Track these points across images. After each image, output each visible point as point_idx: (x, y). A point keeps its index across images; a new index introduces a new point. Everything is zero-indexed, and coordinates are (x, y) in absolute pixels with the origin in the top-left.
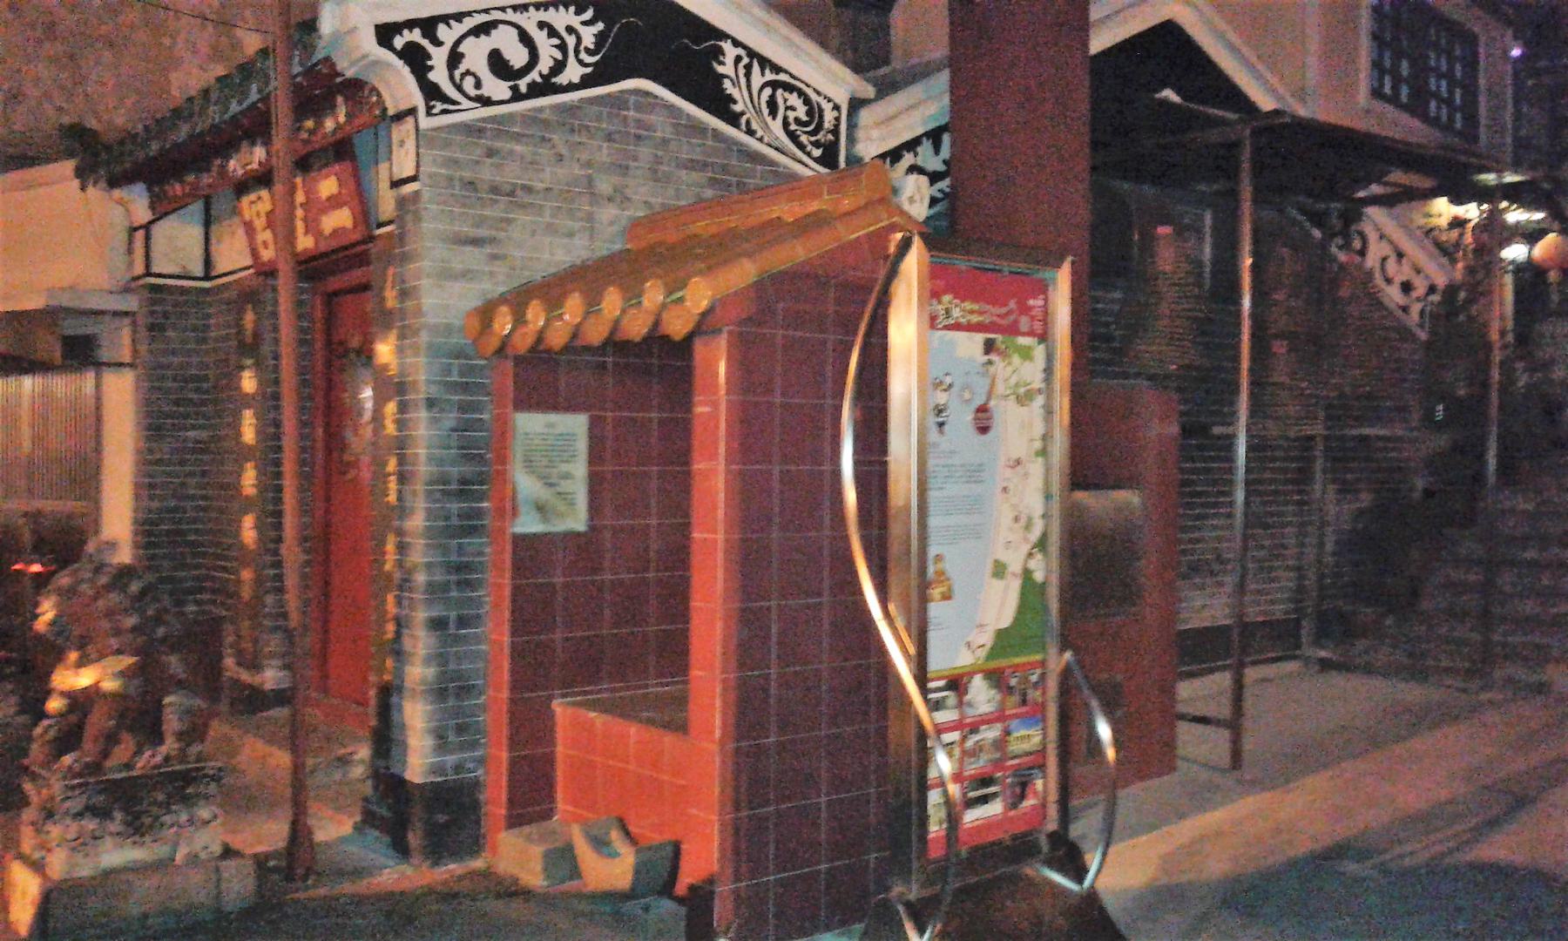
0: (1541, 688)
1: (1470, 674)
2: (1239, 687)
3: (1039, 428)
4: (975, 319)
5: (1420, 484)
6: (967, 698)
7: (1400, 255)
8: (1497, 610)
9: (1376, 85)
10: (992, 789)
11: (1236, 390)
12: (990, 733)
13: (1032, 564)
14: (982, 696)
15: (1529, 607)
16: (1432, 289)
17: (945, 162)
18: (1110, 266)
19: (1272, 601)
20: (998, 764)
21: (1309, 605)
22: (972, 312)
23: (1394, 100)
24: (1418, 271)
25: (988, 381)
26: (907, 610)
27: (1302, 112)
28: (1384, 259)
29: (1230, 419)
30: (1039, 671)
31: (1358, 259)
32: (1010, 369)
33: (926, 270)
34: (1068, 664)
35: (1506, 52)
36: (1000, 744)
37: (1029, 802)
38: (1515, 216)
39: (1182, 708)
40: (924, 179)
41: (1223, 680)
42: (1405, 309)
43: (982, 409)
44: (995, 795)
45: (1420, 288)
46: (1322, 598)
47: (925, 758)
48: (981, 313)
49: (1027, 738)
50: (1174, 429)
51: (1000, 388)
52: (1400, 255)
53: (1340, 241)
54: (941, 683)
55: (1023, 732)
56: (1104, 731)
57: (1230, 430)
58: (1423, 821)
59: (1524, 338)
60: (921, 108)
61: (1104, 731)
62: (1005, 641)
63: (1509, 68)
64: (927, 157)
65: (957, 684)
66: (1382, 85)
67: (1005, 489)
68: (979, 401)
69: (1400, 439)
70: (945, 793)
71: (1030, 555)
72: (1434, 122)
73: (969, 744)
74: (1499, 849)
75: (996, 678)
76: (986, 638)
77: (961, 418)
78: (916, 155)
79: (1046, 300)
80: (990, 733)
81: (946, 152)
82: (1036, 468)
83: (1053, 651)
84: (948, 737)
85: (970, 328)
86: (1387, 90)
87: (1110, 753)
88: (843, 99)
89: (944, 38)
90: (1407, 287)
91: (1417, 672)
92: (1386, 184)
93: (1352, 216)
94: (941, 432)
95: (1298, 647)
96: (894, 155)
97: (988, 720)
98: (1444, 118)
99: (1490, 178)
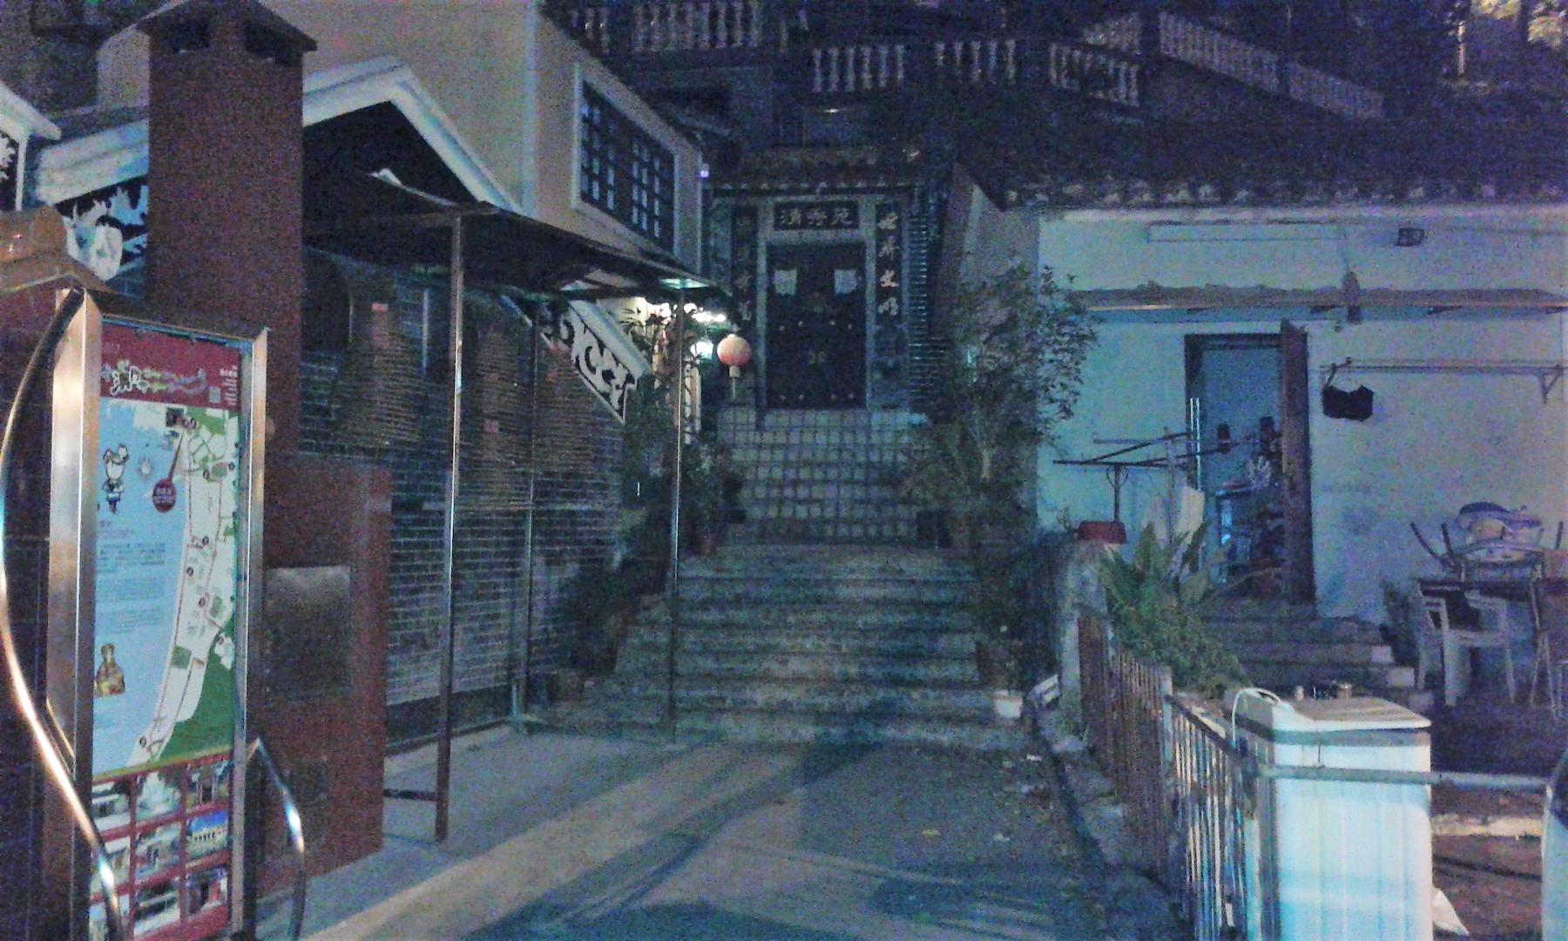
0: (713, 737)
1: (662, 727)
2: (445, 754)
3: (230, 506)
4: (156, 387)
5: (618, 557)
6: (140, 800)
7: (602, 346)
8: (682, 667)
9: (586, 188)
10: (169, 895)
11: (449, 466)
12: (166, 836)
13: (219, 650)
14: (157, 796)
15: (709, 664)
16: (629, 379)
17: (143, 216)
18: (320, 335)
19: (480, 667)
20: (176, 868)
21: (520, 673)
22: (152, 380)
23: (601, 204)
24: (617, 361)
25: (171, 455)
26: (67, 712)
27: (516, 208)
28: (589, 348)
29: (441, 495)
30: (225, 763)
31: (564, 347)
32: (199, 442)
33: (99, 332)
34: (257, 751)
35: (697, 173)
36: (179, 847)
37: (212, 904)
38: (703, 317)
39: (389, 785)
40: (116, 233)
41: (429, 753)
42: (606, 396)
43: (165, 485)
44: (171, 902)
45: (620, 377)
46: (529, 664)
47: (86, 870)
48: (162, 381)
49: (210, 836)
50: (388, 506)
51: (185, 461)
52: (602, 346)
53: (549, 330)
54: (109, 786)
55: (205, 831)
56: (294, 820)
57: (441, 505)
58: (597, 877)
59: (709, 424)
60: (114, 156)
61: (294, 820)
62: (185, 733)
63: (700, 185)
64: (120, 207)
65: (128, 785)
66: (590, 190)
67: (190, 571)
68: (162, 475)
69: (600, 514)
70: (109, 910)
71: (217, 639)
72: (636, 228)
73: (142, 849)
74: (672, 892)
75: (175, 775)
76: (165, 732)
77: (137, 495)
78: (109, 206)
79: (239, 371)
80: (166, 836)
81: (144, 204)
82: (227, 548)
83: (241, 742)
84: (111, 846)
85: (149, 396)
86: (596, 195)
87: (300, 843)
88: (21, 135)
89: (145, 85)
90: (608, 376)
91: (614, 729)
92: (587, 281)
93: (559, 307)
94: (114, 510)
95: (508, 711)
96: (85, 203)
97: (163, 822)
98: (644, 226)
99: (675, 283)
